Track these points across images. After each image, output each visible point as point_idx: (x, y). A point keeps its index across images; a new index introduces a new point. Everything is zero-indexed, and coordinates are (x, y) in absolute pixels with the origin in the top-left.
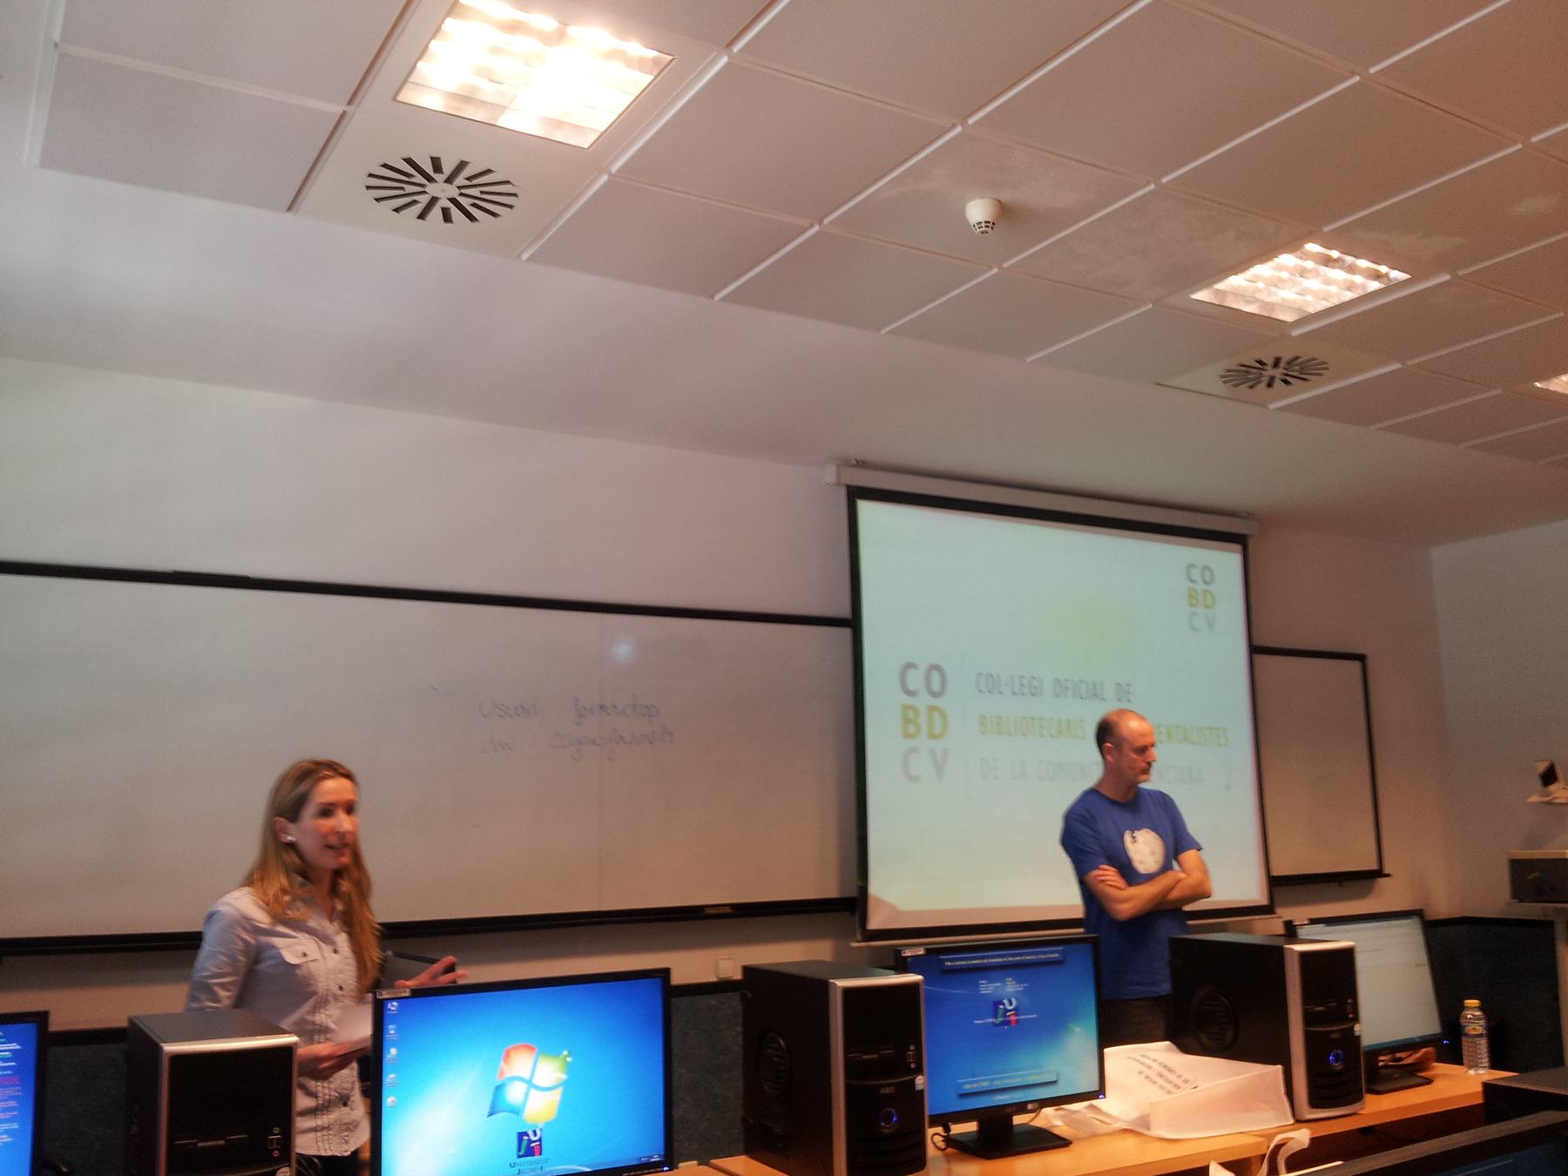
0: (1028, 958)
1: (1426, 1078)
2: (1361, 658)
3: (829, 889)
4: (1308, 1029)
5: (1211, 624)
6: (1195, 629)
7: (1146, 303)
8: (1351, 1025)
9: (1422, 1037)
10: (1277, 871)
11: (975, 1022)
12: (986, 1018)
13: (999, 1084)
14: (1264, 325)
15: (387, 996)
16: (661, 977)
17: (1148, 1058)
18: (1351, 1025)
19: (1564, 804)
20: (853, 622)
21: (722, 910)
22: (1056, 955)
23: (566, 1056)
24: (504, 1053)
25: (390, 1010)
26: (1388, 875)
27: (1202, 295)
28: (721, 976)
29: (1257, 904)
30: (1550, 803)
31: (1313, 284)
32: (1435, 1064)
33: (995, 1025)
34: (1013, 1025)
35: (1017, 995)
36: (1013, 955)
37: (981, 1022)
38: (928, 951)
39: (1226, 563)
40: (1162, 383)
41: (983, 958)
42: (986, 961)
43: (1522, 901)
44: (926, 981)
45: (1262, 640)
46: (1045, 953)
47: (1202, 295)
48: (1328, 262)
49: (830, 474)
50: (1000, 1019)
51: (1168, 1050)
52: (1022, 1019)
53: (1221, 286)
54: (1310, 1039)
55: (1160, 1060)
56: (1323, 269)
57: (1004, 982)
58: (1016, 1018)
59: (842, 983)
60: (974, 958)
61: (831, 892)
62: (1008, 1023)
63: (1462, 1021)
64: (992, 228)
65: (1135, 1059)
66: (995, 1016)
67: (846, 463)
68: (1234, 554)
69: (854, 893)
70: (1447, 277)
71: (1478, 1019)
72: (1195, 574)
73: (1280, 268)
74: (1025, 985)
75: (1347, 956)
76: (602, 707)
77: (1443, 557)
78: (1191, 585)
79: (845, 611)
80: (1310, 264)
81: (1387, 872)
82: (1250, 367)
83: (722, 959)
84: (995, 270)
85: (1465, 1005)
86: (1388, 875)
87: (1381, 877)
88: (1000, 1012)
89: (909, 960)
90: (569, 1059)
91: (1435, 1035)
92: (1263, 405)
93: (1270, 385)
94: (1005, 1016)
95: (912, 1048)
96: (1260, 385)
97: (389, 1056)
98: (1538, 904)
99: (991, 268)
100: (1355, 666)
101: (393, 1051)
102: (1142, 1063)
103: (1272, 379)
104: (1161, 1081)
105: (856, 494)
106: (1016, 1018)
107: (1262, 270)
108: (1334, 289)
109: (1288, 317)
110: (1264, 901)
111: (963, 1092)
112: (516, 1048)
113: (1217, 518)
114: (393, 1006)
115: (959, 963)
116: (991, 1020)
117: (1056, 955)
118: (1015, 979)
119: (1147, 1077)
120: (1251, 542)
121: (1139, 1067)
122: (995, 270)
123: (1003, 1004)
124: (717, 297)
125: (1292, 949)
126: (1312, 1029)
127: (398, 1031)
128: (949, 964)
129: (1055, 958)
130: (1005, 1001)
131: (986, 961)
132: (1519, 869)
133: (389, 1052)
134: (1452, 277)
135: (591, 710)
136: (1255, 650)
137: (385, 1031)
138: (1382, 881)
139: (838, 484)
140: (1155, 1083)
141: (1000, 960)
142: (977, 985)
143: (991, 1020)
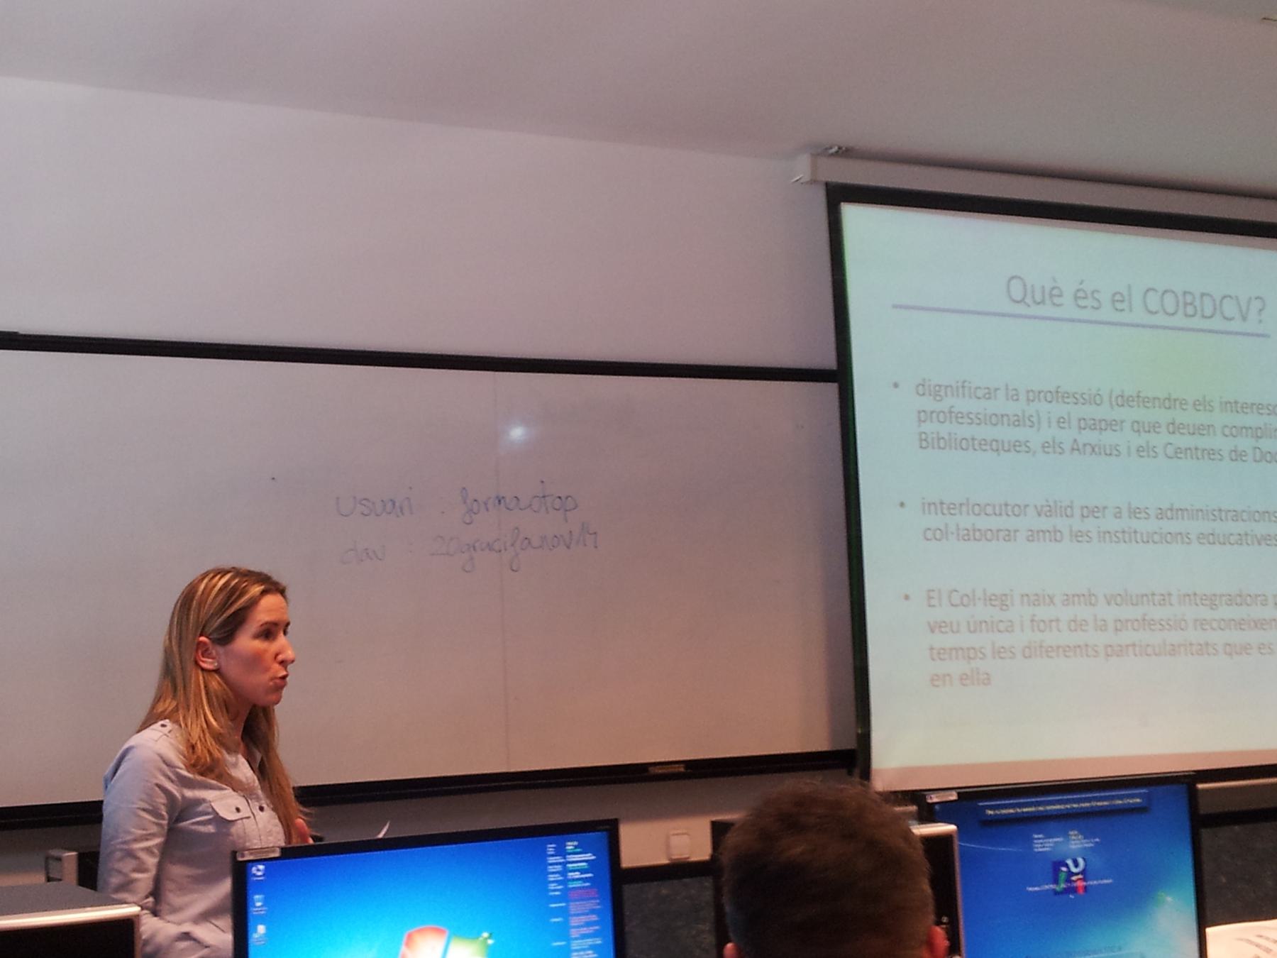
0: (1099, 804)
15: (251, 858)
16: (606, 830)
23: (486, 939)
24: (405, 938)
25: (255, 875)
28: (674, 857)
33: (1056, 893)
34: (1081, 892)
35: (1085, 853)
37: (1036, 889)
41: (1038, 804)
42: (1041, 808)
49: (802, 168)
50: (1063, 886)
52: (1091, 886)
57: (1066, 835)
58: (1085, 883)
61: (819, 743)
62: (1071, 890)
66: (1056, 881)
67: (822, 152)
69: (849, 744)
74: (1097, 840)
76: (500, 500)
79: (828, 360)
83: (674, 835)
88: (1063, 876)
89: (937, 807)
90: (490, 942)
94: (1068, 880)
97: (255, 936)
101: (261, 929)
102: (1258, 946)
105: (839, 195)
106: (1085, 883)
112: (420, 931)
114: (258, 870)
115: (1004, 811)
117: (1138, 800)
118: (1081, 832)
123: (1067, 866)
127: (266, 902)
128: (990, 812)
130: (1070, 862)
131: (1041, 808)
133: (256, 931)
135: (486, 504)
137: (250, 904)
139: (813, 182)
141: (1062, 807)
143: (1052, 886)
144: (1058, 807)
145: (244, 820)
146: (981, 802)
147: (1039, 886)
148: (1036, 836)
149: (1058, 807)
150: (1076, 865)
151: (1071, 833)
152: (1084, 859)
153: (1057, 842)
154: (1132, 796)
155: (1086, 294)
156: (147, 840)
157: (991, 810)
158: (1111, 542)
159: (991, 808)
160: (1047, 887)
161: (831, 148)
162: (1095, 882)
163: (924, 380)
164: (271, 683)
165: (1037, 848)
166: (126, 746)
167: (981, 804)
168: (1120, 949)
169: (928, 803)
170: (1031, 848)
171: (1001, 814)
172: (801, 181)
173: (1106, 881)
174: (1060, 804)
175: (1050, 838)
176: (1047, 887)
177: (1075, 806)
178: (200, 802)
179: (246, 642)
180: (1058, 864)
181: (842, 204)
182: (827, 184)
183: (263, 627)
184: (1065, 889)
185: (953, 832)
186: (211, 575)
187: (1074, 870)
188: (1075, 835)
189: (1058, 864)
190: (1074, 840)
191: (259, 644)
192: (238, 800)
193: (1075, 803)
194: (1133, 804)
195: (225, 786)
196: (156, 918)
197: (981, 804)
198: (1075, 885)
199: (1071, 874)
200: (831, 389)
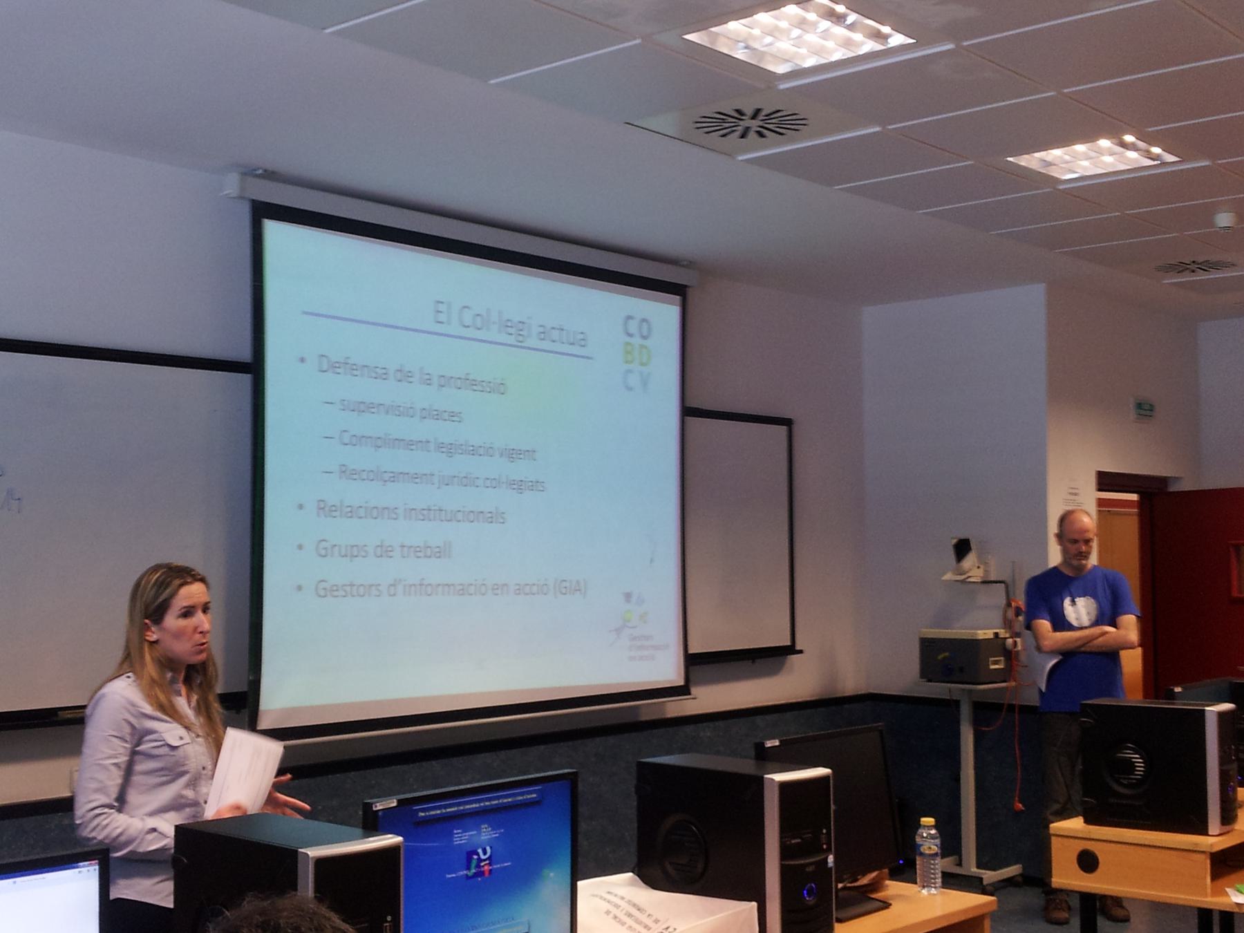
2: (787, 422)
4: (783, 863)
5: (645, 383)
6: (630, 389)
7: (635, 39)
10: (693, 650)
14: (755, 74)
17: (616, 895)
19: (977, 582)
20: (254, 368)
22: (534, 796)
26: (801, 652)
30: (963, 582)
32: (888, 882)
33: (468, 877)
36: (489, 799)
38: (399, 801)
43: (930, 681)
44: (405, 840)
45: (693, 403)
46: (522, 794)
49: (231, 184)
50: (473, 871)
51: (632, 884)
54: (786, 874)
55: (628, 897)
56: (825, 24)
57: (478, 828)
58: (490, 868)
59: (314, 852)
60: (446, 807)
62: (480, 874)
63: (918, 840)
65: (601, 898)
67: (249, 172)
68: (670, 306)
71: (932, 838)
72: (633, 326)
74: (502, 831)
78: (628, 339)
79: (244, 353)
80: (812, 16)
81: (798, 648)
85: (921, 823)
86: (801, 652)
87: (794, 654)
88: (474, 863)
89: (380, 813)
92: (730, 155)
94: (478, 866)
95: (389, 918)
98: (945, 684)
103: (747, 129)
104: (629, 921)
105: (263, 211)
108: (830, 44)
109: (781, 69)
110: (680, 682)
113: (651, 263)
115: (433, 813)
117: (534, 796)
119: (615, 917)
120: (690, 292)
121: (606, 906)
123: (478, 854)
125: (772, 780)
126: (787, 863)
128: (423, 814)
129: (533, 798)
130: (480, 851)
132: (928, 646)
136: (688, 411)
140: (623, 924)
142: (451, 834)
143: (465, 872)
144: (474, 806)
145: (185, 746)
146: (415, 806)
147: (455, 873)
148: (455, 832)
149: (474, 806)
151: (483, 826)
152: (491, 848)
153: (472, 835)
154: (530, 793)
156: (116, 758)
157: (422, 812)
158: (475, 585)
159: (423, 810)
160: (462, 873)
161: (255, 170)
162: (499, 866)
164: (193, 649)
165: (456, 841)
166: (1053, 528)
167: (415, 808)
169: (373, 811)
171: (430, 815)
173: (506, 864)
174: (476, 803)
175: (466, 832)
176: (462, 873)
177: (487, 803)
178: (151, 732)
179: (172, 621)
182: (253, 201)
183: (183, 611)
184: (475, 873)
186: (150, 572)
187: (483, 857)
188: (486, 828)
190: (484, 832)
191: (183, 622)
192: (182, 731)
193: (487, 801)
194: (530, 799)
195: (168, 719)
196: (121, 815)
197: (415, 808)
198: (482, 869)
199: (480, 860)
200: (245, 379)
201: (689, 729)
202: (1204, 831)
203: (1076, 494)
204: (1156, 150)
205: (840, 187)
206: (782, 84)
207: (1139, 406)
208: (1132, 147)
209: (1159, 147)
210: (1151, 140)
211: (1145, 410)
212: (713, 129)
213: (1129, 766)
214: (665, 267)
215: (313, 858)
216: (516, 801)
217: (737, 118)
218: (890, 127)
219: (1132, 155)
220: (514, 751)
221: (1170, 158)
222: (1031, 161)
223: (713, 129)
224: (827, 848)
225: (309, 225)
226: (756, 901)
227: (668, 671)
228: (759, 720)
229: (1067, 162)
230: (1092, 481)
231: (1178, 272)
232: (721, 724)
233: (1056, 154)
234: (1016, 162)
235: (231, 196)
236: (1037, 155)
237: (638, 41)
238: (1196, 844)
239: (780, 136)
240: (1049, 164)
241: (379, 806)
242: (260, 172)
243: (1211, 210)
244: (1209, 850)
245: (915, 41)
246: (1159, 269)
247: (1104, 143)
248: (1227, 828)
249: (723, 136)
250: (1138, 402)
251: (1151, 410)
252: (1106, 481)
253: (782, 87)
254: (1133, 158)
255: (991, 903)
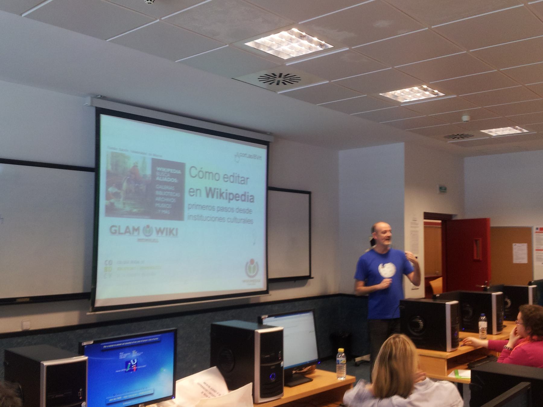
0: (144, 341)
1: (424, 96)
2: (309, 193)
3: (79, 289)
8: (280, 362)
9: (309, 361)
10: (271, 276)
11: (116, 371)
12: (121, 369)
13: (125, 397)
14: (274, 59)
18: (280, 362)
21: (24, 300)
27: (250, 44)
29: (262, 290)
31: (295, 45)
34: (134, 371)
38: (95, 342)
39: (261, 151)
40: (234, 78)
47: (250, 44)
48: (302, 37)
50: (128, 369)
53: (257, 41)
57: (132, 352)
58: (136, 368)
59: (46, 363)
60: (117, 343)
64: (153, 2)
70: (348, 49)
73: (282, 37)
75: (280, 334)
77: (342, 154)
79: (92, 165)
80: (294, 37)
82: (269, 76)
84: (158, 20)
86: (313, 278)
89: (85, 347)
91: (315, 360)
93: (278, 84)
96: (285, 75)
99: (156, 19)
100: (307, 195)
105: (100, 111)
107: (275, 37)
109: (286, 58)
110: (265, 289)
111: (108, 403)
116: (124, 370)
120: (271, 145)
122: (158, 20)
124: (23, 16)
130: (132, 361)
134: (349, 48)
136: (269, 188)
138: (310, 280)
139: (92, 106)
142: (118, 355)
143: (124, 370)
144: (129, 343)
149: (129, 343)
150: (134, 362)
155: (194, 190)
159: (106, 345)
161: (98, 96)
163: (234, 173)
168: (146, 388)
170: (119, 357)
172: (87, 105)
176: (123, 370)
180: (127, 363)
181: (101, 114)
182: (96, 107)
185: (86, 360)
189: (127, 363)
194: (155, 340)
198: (132, 369)
199: (131, 365)
200: (92, 174)
201: (269, 307)
202: (445, 350)
203: (416, 220)
204: (436, 91)
205: (353, 114)
206: (288, 63)
207: (441, 188)
208: (425, 90)
209: (437, 90)
210: (433, 87)
211: (443, 189)
212: (263, 79)
213: (418, 325)
214: (257, 134)
215: (45, 366)
216: (148, 341)
217: (274, 77)
218: (332, 81)
219: (427, 93)
220: (199, 315)
221: (441, 94)
222: (390, 95)
223: (263, 79)
224: (280, 359)
225: (122, 117)
226: (251, 382)
227: (260, 285)
228: (296, 303)
229: (402, 96)
230: (422, 216)
231: (453, 138)
232: (282, 305)
233: (398, 92)
234: (383, 95)
235: (89, 105)
236: (391, 92)
237: (228, 45)
238: (441, 355)
239: (291, 84)
240: (396, 97)
241: (85, 344)
242: (100, 96)
243: (460, 115)
244: (446, 357)
245: (333, 47)
246: (445, 137)
247: (416, 88)
248: (454, 349)
249: (270, 84)
250: (440, 186)
251: (445, 190)
252: (427, 216)
253: (287, 64)
254: (428, 94)
255: (354, 379)
